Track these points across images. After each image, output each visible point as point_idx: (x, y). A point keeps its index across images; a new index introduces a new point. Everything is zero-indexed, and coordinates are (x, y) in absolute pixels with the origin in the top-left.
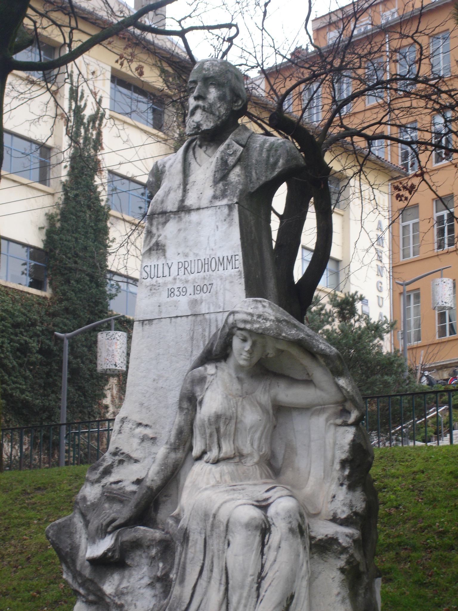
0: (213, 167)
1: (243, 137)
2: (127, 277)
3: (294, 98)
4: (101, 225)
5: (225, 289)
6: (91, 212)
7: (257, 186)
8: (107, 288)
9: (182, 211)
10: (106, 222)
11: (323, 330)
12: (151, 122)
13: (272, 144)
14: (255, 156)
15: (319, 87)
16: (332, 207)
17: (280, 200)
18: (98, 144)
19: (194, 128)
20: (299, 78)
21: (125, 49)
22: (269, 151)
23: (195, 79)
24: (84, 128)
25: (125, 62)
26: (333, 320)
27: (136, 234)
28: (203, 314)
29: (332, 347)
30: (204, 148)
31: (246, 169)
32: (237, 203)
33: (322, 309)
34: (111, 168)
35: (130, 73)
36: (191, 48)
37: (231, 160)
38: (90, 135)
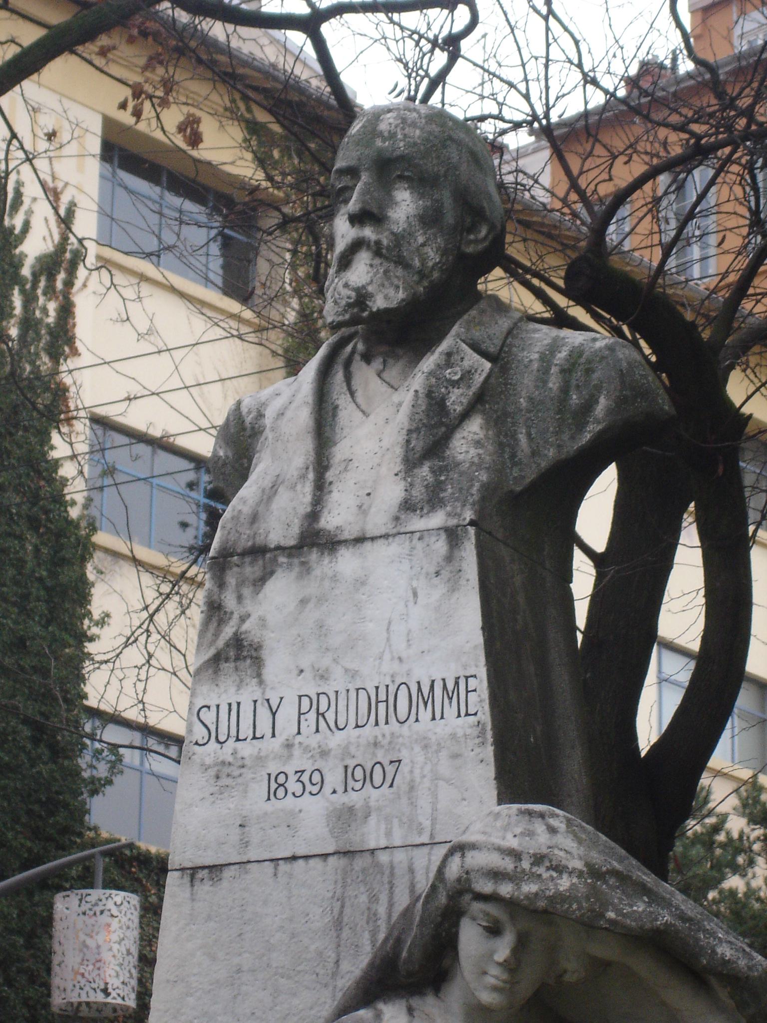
0: (402, 419)
1: (491, 331)
2: (146, 730)
3: (640, 214)
4: (66, 575)
5: (436, 778)
6: (40, 536)
7: (531, 475)
8: (84, 761)
9: (313, 545)
10: (83, 567)
11: (721, 892)
12: (219, 281)
13: (576, 354)
14: (525, 385)
15: (712, 182)
16: (751, 528)
17: (596, 515)
18: (62, 339)
19: (349, 305)
20: (652, 155)
21: (145, 68)
22: (566, 371)
23: (353, 163)
24: (23, 291)
25: (147, 105)
26: (751, 863)
27: (172, 607)
28: (372, 851)
29: (755, 954)
30: (377, 364)
31: (501, 424)
32: (472, 523)
33: (717, 829)
34: (101, 411)
35: (158, 135)
36: (339, 62)
37: (457, 399)
38: (38, 314)
